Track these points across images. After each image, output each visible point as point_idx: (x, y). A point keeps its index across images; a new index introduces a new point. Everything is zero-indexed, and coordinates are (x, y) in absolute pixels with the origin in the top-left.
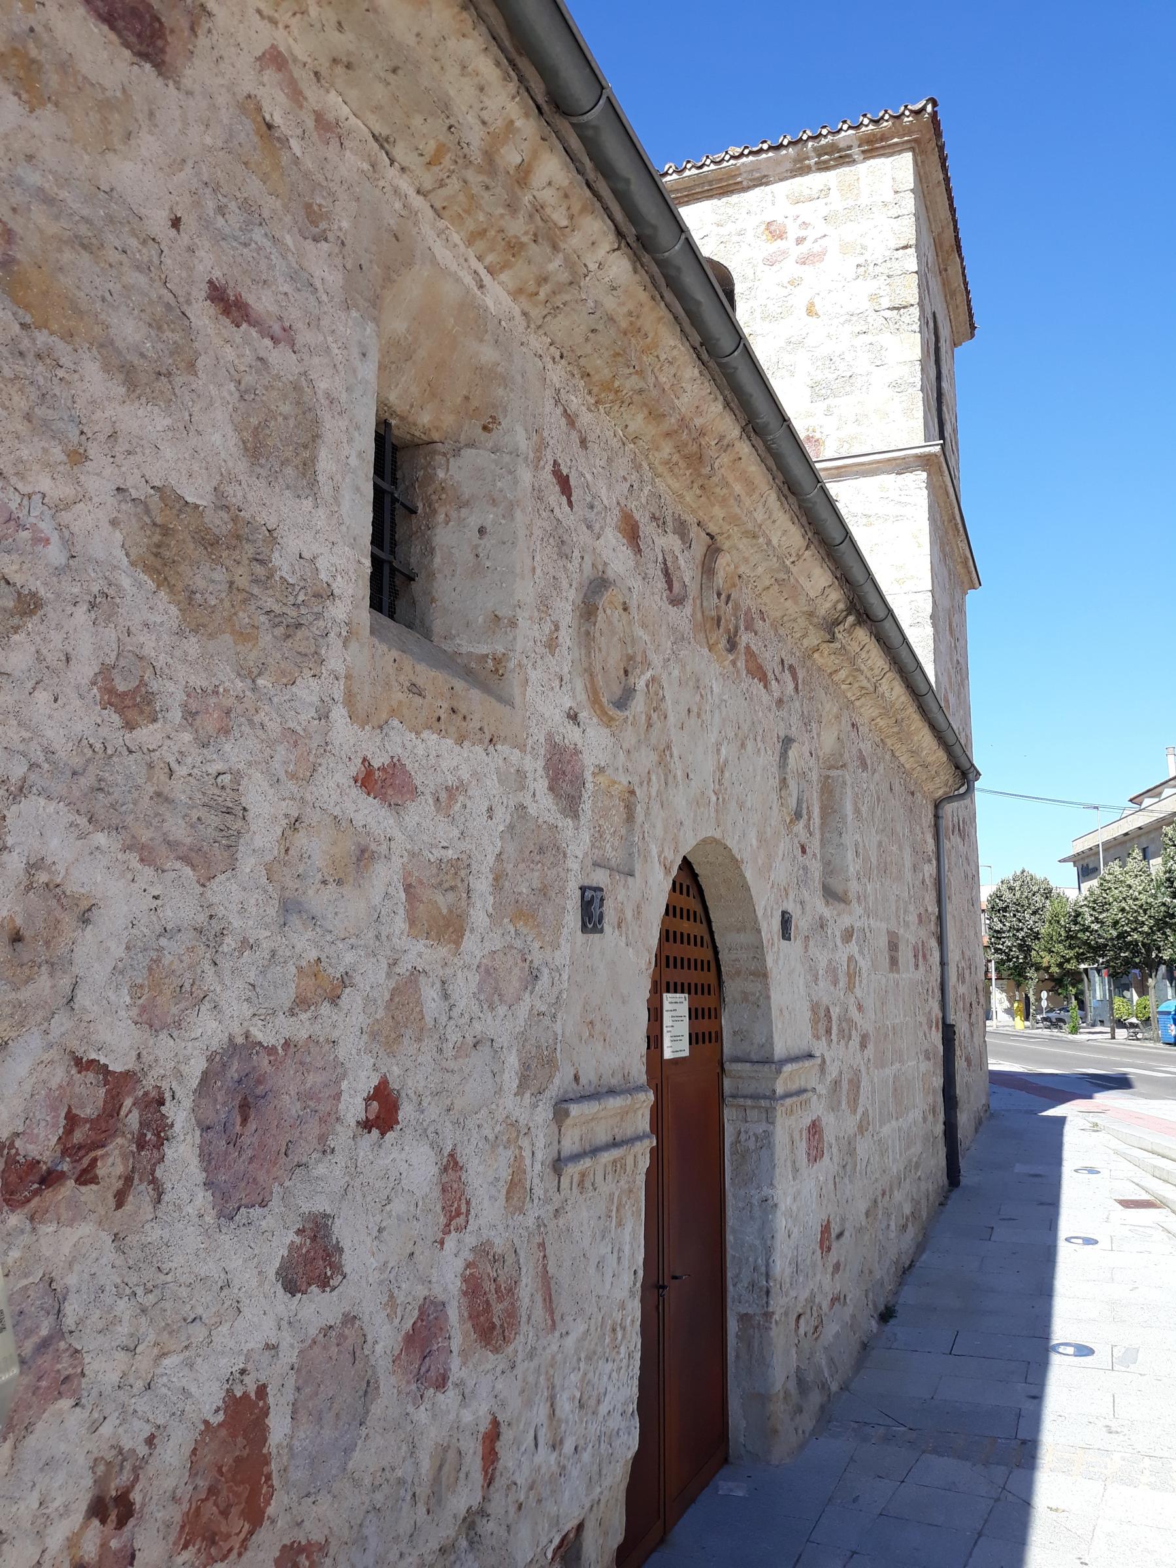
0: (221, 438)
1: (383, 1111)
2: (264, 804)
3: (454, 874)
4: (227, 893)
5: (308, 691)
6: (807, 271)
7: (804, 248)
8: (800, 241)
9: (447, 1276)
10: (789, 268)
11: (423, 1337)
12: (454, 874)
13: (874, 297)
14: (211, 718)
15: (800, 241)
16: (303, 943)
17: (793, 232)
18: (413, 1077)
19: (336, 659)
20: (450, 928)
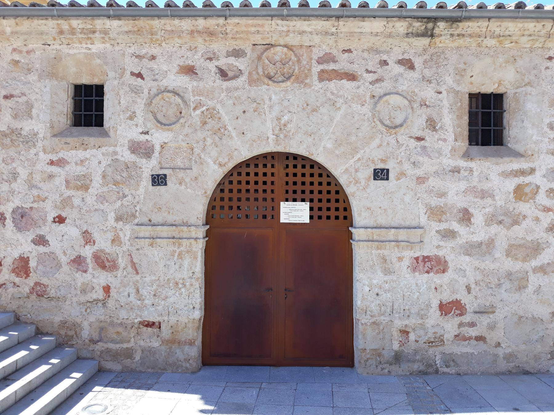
5: (33, 151)
16: (35, 192)
19: (40, 144)
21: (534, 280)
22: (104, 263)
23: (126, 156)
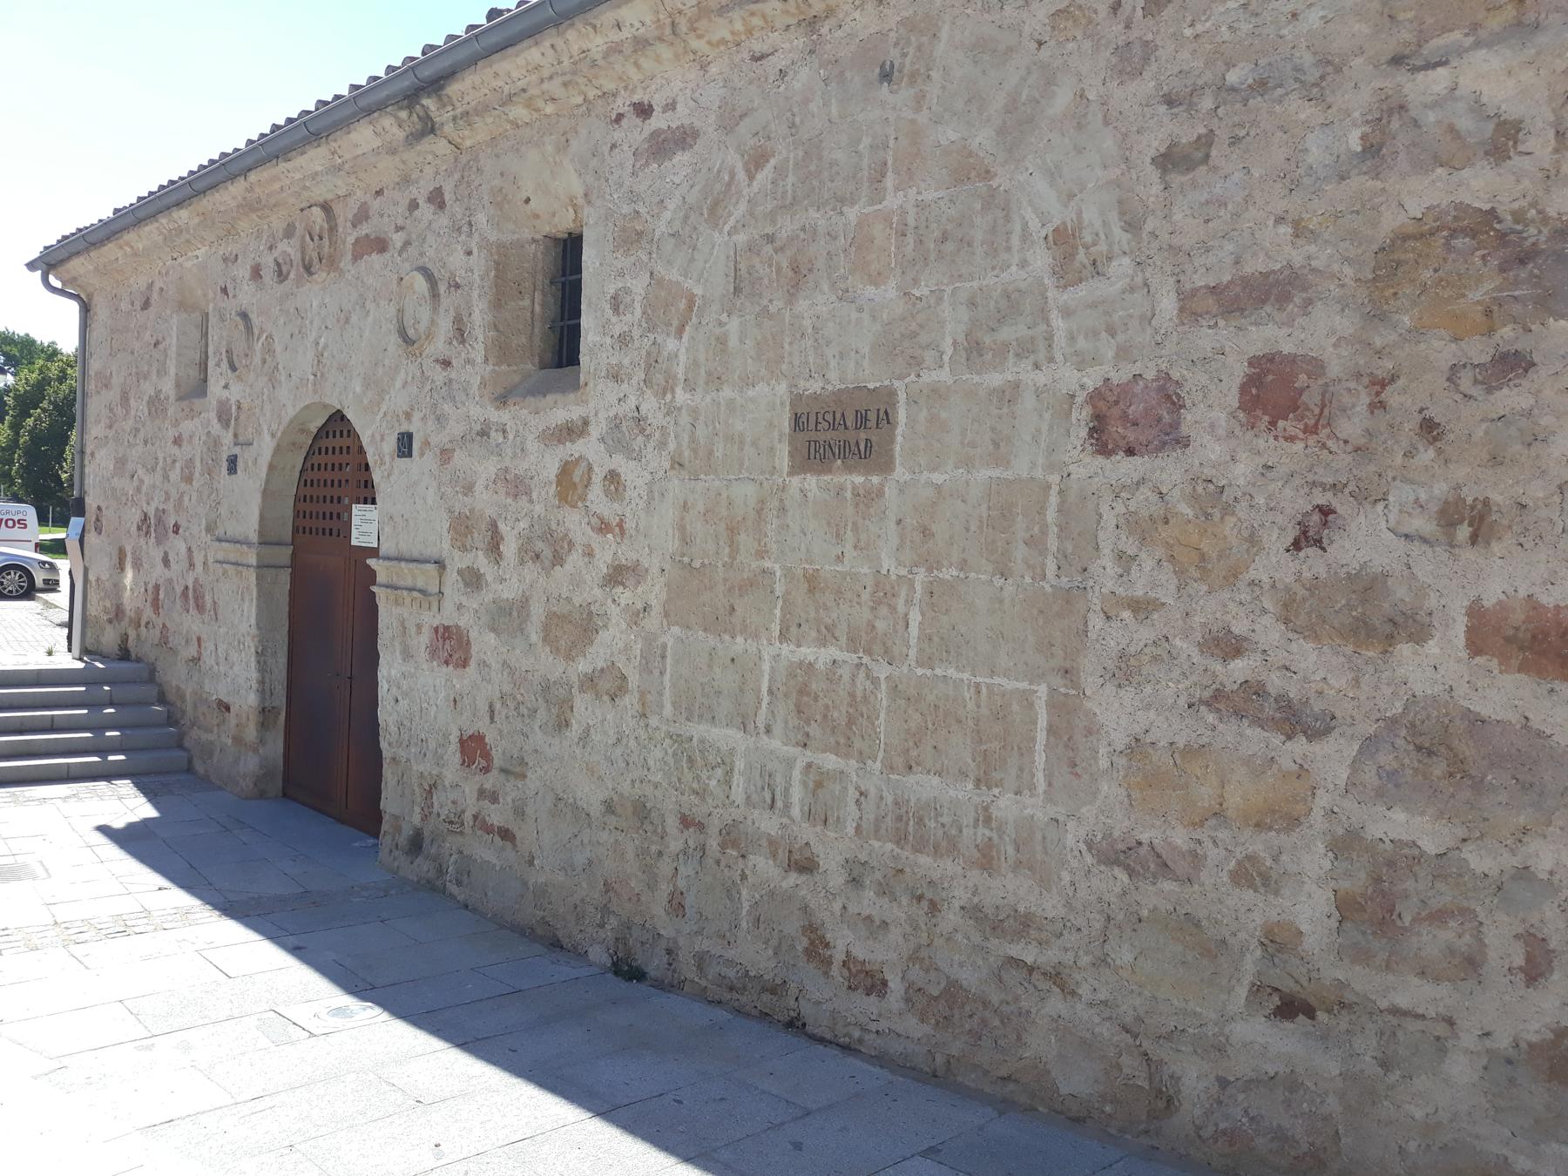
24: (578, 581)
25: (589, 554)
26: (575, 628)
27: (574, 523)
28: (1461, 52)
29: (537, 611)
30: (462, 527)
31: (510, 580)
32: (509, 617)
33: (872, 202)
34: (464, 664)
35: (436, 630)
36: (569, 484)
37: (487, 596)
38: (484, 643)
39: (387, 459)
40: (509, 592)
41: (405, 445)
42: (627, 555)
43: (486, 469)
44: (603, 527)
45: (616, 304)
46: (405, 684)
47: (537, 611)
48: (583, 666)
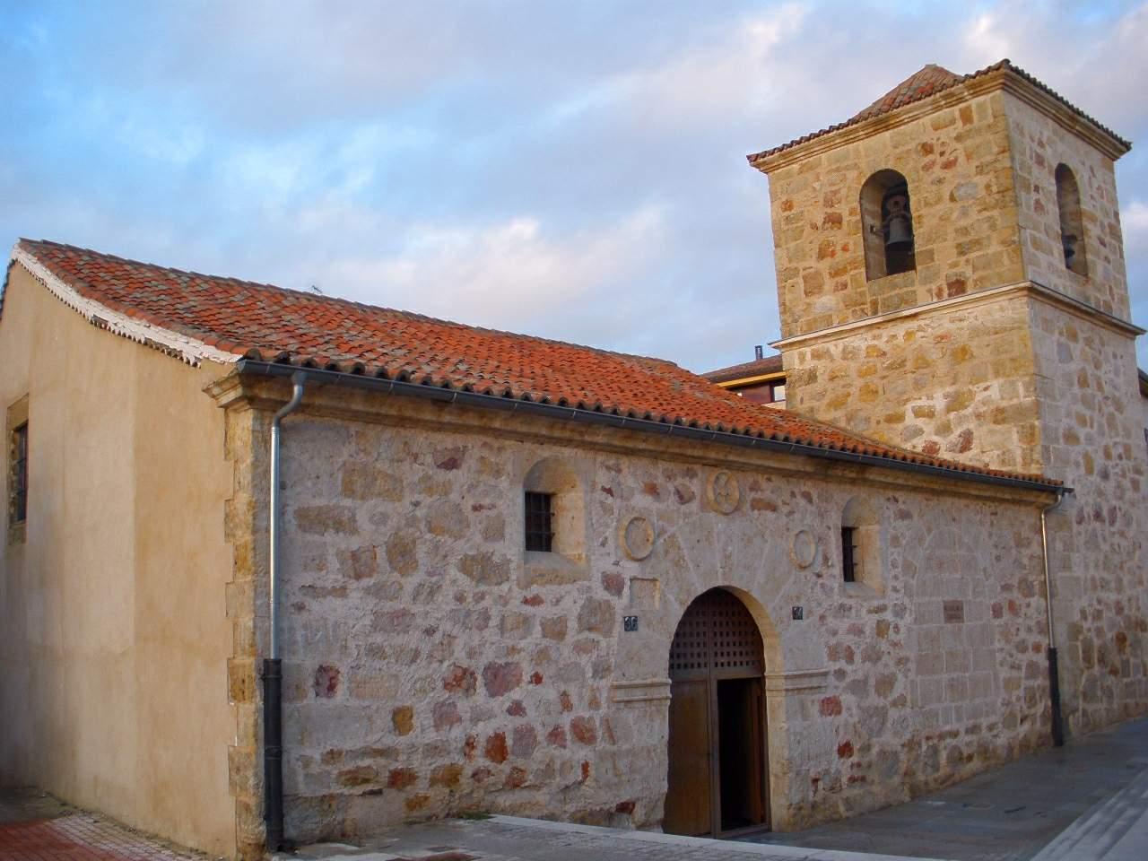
0: (478, 538)
1: (537, 679)
2: (494, 612)
3: (561, 621)
4: (486, 633)
6: (948, 174)
7: (944, 159)
8: (942, 154)
9: (566, 720)
10: (938, 172)
11: (556, 735)
12: (561, 621)
13: (988, 187)
14: (480, 597)
15: (942, 154)
17: (937, 149)
18: (547, 672)
20: (561, 635)
21: (893, 713)
22: (583, 734)
23: (601, 594)
24: (888, 665)
25: (896, 627)
26: (886, 684)
27: (884, 646)
28: (886, 236)
29: (872, 682)
30: (833, 654)
31: (856, 670)
32: (859, 687)
33: (968, 108)
34: (839, 712)
35: (823, 701)
36: (881, 629)
37: (848, 680)
38: (847, 699)
39: (785, 620)
40: (860, 676)
41: (797, 614)
42: (902, 654)
43: (843, 625)
44: (895, 645)
45: (1039, 206)
46: (805, 733)
47: (872, 682)
48: (890, 699)
